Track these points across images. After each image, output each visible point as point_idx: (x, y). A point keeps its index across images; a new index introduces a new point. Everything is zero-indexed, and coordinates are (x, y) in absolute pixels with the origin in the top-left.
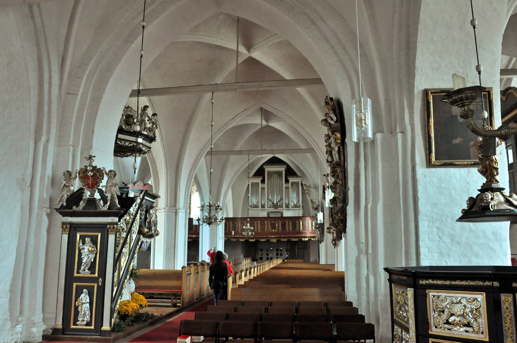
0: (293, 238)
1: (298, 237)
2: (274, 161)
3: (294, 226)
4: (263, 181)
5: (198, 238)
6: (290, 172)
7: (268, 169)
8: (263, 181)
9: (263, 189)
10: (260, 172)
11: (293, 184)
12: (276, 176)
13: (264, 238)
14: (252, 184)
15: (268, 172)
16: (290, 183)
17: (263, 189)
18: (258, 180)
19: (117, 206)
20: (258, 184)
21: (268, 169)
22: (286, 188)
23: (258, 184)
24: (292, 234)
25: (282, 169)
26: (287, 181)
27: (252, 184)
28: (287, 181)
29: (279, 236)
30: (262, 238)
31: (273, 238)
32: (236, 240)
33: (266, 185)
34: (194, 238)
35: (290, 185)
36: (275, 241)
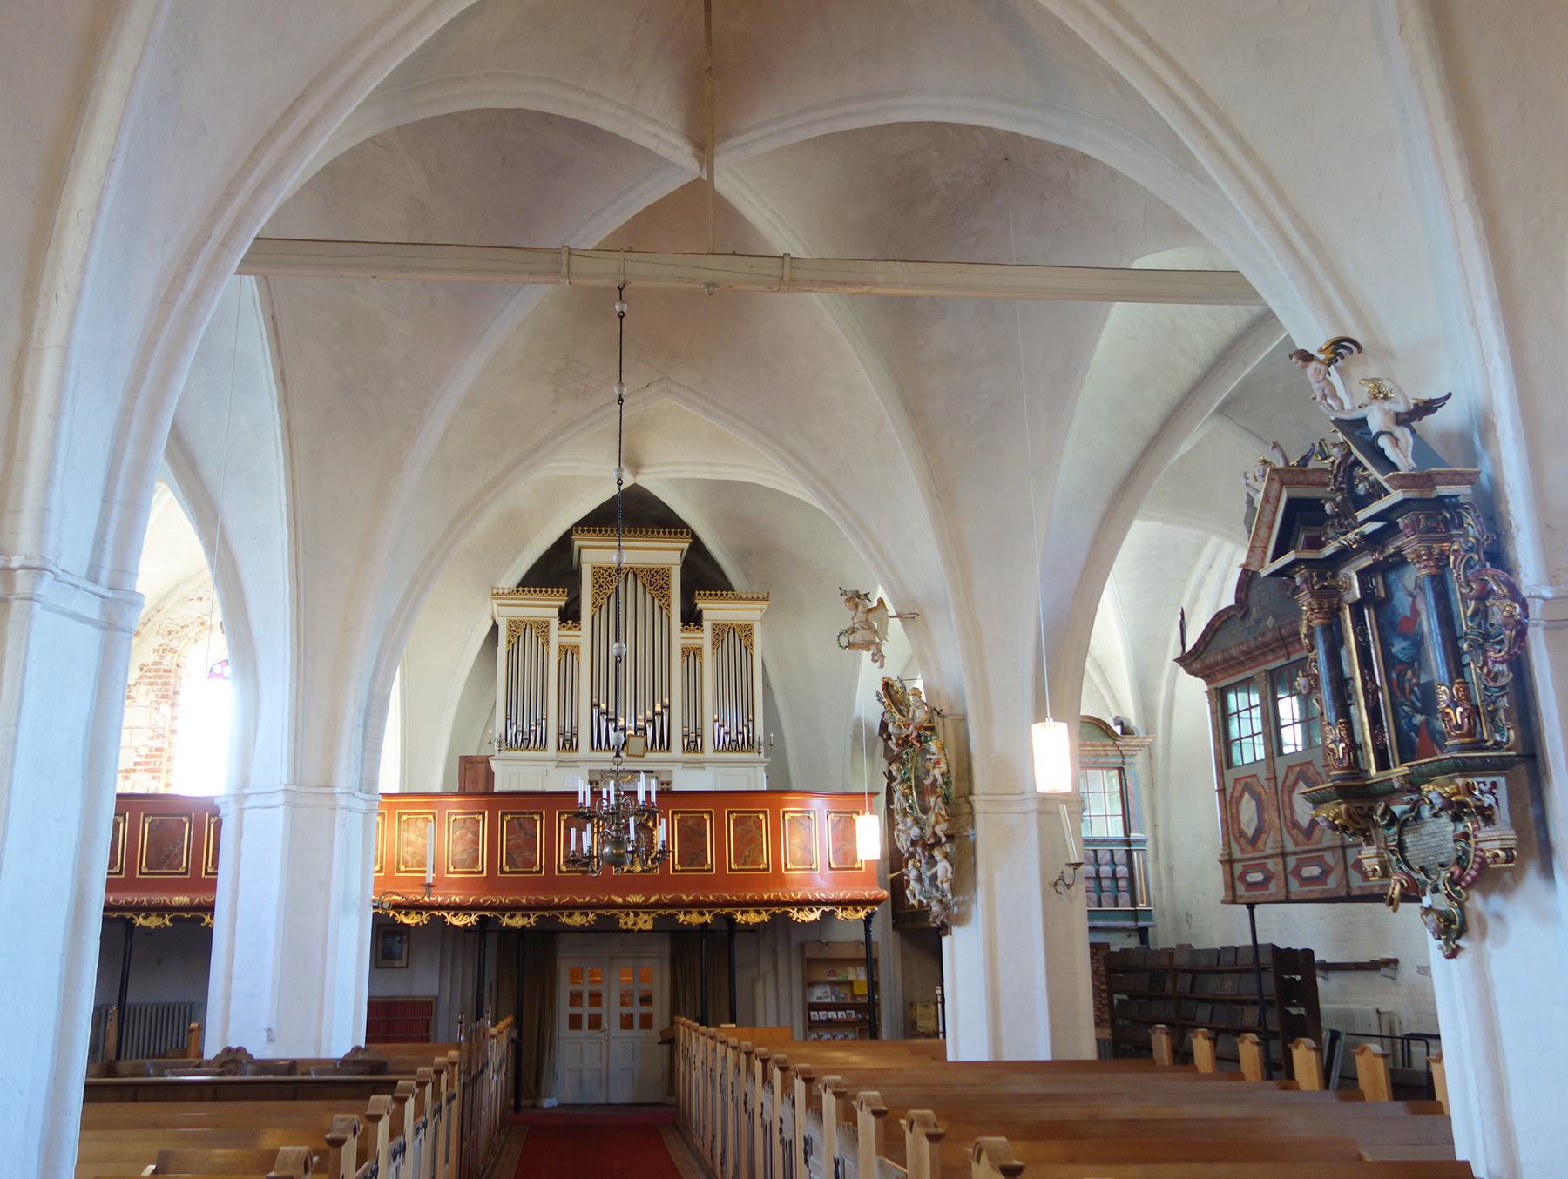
0: (149, 909)
1: (769, 904)
2: (632, 513)
3: (748, 841)
4: (570, 615)
5: (210, 908)
6: (702, 575)
7: (594, 554)
8: (570, 615)
9: (569, 652)
10: (554, 569)
11: (720, 631)
12: (634, 594)
13: (584, 908)
14: (513, 625)
15: (598, 571)
16: (707, 625)
17: (569, 652)
18: (546, 608)
19: (860, 698)
20: (544, 627)
21: (594, 554)
22: (564, 650)
23: (544, 627)
24: (145, 886)
25: (667, 555)
26: (692, 617)
27: (513, 625)
28: (692, 617)
29: (667, 897)
30: (571, 908)
31: (636, 906)
32: (423, 919)
33: (582, 636)
34: (182, 908)
35: (705, 638)
36: (645, 922)
